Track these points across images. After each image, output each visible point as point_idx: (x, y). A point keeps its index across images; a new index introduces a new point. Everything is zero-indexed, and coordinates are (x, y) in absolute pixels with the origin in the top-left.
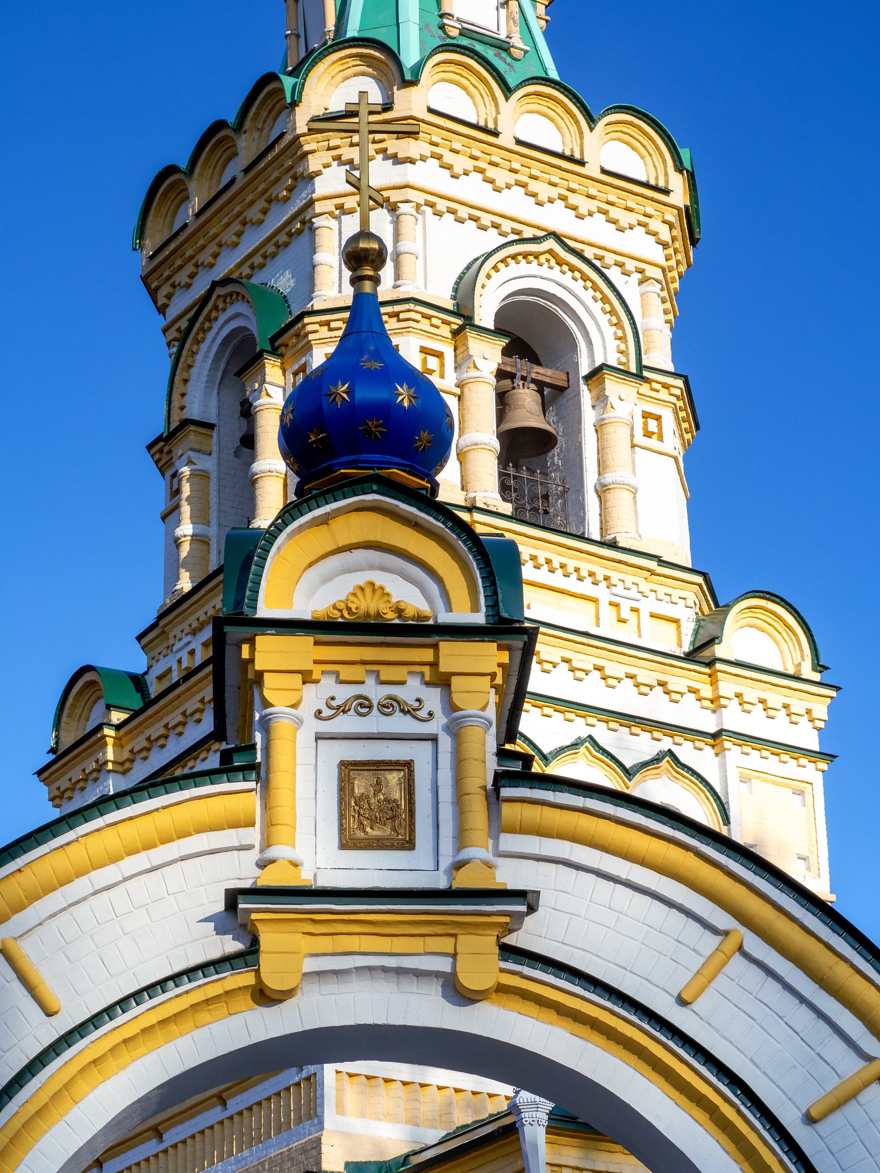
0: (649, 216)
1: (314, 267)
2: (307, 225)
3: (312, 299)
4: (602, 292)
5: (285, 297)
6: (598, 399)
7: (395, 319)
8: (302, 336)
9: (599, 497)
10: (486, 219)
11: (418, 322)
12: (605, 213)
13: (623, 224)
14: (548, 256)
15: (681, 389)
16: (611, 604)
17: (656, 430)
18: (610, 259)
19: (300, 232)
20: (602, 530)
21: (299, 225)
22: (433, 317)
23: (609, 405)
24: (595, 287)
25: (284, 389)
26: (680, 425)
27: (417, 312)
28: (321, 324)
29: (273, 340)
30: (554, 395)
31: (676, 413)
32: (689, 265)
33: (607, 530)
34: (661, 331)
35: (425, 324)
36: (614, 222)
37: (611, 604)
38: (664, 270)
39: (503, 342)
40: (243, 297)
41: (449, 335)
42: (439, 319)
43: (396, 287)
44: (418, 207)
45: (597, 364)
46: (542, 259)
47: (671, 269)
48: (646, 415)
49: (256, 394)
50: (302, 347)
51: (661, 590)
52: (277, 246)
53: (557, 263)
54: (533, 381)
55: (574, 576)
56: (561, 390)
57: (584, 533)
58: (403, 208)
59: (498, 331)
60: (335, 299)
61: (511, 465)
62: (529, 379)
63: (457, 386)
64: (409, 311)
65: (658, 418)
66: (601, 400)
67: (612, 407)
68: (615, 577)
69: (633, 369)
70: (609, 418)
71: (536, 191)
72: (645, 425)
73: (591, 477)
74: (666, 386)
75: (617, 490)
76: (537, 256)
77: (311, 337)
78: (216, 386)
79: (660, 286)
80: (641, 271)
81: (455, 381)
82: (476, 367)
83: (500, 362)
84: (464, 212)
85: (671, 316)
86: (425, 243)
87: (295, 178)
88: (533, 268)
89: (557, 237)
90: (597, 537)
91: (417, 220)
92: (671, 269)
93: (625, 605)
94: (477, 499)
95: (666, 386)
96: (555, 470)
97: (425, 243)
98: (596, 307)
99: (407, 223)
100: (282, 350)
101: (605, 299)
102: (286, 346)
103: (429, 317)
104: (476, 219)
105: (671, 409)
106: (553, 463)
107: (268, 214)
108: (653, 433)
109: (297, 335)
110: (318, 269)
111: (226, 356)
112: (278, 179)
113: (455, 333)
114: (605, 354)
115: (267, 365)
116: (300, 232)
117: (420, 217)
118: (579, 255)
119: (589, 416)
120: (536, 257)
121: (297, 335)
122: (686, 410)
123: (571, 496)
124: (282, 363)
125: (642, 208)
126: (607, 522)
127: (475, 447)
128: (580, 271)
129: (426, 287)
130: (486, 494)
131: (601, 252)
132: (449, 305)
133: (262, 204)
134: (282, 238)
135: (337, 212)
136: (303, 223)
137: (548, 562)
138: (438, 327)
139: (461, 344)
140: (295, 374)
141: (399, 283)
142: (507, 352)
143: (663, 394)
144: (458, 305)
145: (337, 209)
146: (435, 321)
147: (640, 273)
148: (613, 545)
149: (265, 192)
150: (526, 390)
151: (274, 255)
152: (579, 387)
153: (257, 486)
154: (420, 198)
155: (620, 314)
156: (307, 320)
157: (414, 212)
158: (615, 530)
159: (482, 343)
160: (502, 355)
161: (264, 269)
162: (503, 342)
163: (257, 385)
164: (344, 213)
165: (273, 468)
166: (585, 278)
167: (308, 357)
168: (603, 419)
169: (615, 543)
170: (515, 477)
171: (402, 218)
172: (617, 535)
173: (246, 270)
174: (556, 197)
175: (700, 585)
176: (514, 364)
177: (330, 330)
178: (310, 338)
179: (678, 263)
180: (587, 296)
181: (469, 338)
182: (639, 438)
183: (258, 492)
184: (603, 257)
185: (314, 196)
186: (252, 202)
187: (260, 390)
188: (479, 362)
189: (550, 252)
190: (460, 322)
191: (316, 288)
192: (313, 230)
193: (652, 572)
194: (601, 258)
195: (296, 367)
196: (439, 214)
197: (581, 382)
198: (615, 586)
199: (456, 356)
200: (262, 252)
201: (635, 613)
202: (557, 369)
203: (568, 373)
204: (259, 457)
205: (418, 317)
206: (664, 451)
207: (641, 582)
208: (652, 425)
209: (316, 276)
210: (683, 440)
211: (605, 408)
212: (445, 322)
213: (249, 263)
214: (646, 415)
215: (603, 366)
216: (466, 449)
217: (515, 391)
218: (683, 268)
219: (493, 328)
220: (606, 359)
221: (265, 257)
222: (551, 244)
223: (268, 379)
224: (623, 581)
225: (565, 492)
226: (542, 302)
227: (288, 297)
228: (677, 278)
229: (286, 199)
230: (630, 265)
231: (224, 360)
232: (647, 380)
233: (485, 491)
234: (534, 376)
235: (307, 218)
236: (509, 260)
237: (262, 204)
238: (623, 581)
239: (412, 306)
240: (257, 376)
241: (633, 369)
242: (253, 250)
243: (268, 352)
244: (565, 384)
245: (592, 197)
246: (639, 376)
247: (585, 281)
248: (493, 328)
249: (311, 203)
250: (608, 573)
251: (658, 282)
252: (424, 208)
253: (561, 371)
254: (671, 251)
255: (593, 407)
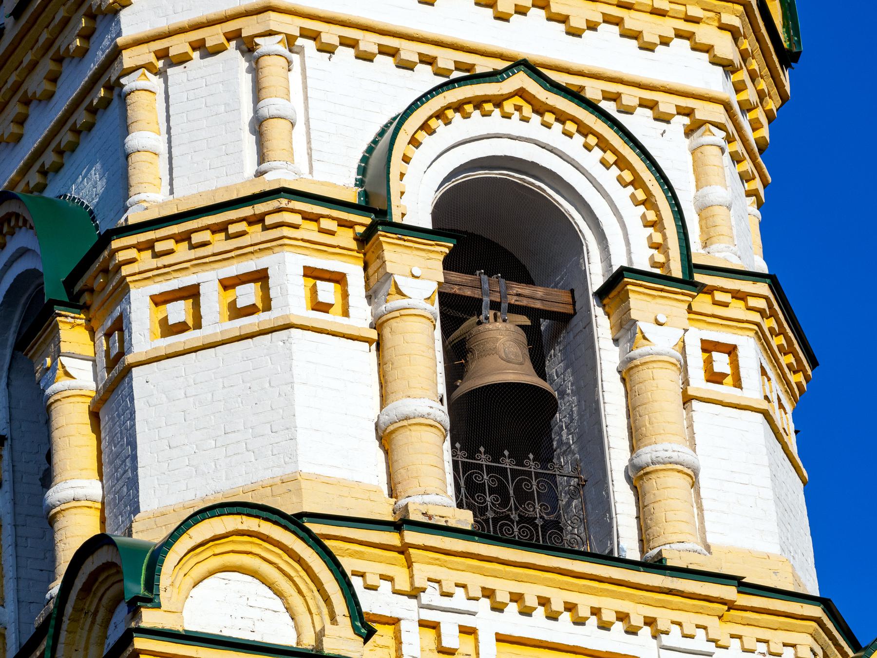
0: (696, 21)
1: (127, 156)
2: (116, 91)
3: (126, 209)
4: (615, 152)
5: (91, 212)
6: (621, 326)
7: (259, 227)
8: (111, 271)
9: (634, 488)
10: (410, 51)
11: (296, 227)
12: (618, 22)
13: (650, 37)
14: (518, 101)
15: (767, 298)
16: (423, 624)
17: (727, 370)
18: (631, 97)
19: (106, 103)
20: (643, 542)
21: (102, 93)
22: (323, 216)
23: (639, 335)
24: (604, 144)
25: (94, 361)
26: (777, 360)
27: (293, 211)
28: (140, 247)
29: (70, 282)
30: (553, 332)
31: (762, 337)
32: (784, 98)
33: (649, 541)
34: (729, 208)
35: (309, 231)
36: (635, 36)
37: (423, 624)
38: (728, 107)
39: (444, 248)
40: (25, 221)
41: (354, 245)
42: (333, 219)
43: (259, 174)
44: (290, 41)
45: (615, 269)
46: (508, 106)
47: (746, 108)
48: (708, 347)
49: (49, 374)
50: (115, 289)
51: (750, 634)
52: (77, 132)
53: (535, 111)
54: (514, 309)
55: (593, 621)
56: (562, 320)
57: (612, 551)
58: (265, 45)
59: (436, 233)
60: (161, 206)
61: (482, 449)
62: (504, 306)
63: (373, 326)
64: (279, 210)
65: (731, 350)
66: (626, 329)
67: (645, 338)
68: (664, 618)
69: (677, 271)
70: (641, 356)
71: (712, 43)
72: (709, 362)
73: (618, 457)
74: (738, 295)
75: (661, 474)
76: (498, 102)
77: (125, 270)
78: (5, 374)
79: (724, 134)
80: (688, 113)
81: (370, 320)
82: (400, 293)
83: (442, 280)
84: (369, 42)
85: (757, 184)
86: (306, 98)
87: (92, 16)
88: (495, 122)
89: (531, 68)
90: (633, 553)
91: (289, 63)
92: (746, 108)
93: (450, 626)
94: (411, 509)
95: (738, 295)
96: (564, 453)
97: (306, 98)
98: (609, 178)
99: (272, 68)
100: (86, 298)
101: (622, 163)
102: (91, 291)
103: (316, 218)
104: (393, 53)
105: (752, 334)
106: (560, 442)
107: (59, 82)
108: (725, 375)
109: (105, 271)
110: (133, 158)
111: (14, 324)
112: (66, 22)
113: (363, 240)
114: (629, 252)
115: (61, 325)
116: (106, 103)
117: (295, 58)
118: (576, 96)
119: (609, 357)
120: (498, 105)
121: (105, 271)
122: (782, 332)
123: (590, 491)
124: (88, 320)
125: (682, 8)
126: (648, 528)
127: (405, 423)
128: (574, 120)
129: (311, 172)
130: (426, 498)
131: (613, 88)
132: (352, 195)
133: (47, 65)
134: (81, 117)
135: (160, 64)
136: (109, 88)
137: (544, 602)
138: (332, 233)
139: (374, 256)
140: (108, 335)
141: (265, 166)
142: (449, 264)
143: (737, 310)
144: (366, 195)
145: (158, 59)
146: (325, 224)
147: (687, 115)
148: (657, 565)
149: (50, 44)
150: (499, 325)
151: (73, 147)
152: (589, 310)
153: (57, 526)
154: (291, 25)
155: (649, 184)
156: (115, 244)
157: (283, 49)
158: (662, 540)
159: (408, 251)
160: (444, 269)
161: (63, 171)
162: (444, 248)
163: (49, 361)
164: (172, 64)
165: (80, 493)
166: (584, 130)
167: (124, 304)
168: (632, 359)
169: (661, 560)
170: (490, 469)
171: (264, 61)
172: (663, 548)
173: (34, 178)
174: (672, 34)
175: (818, 621)
176: (477, 284)
177: (156, 255)
178: (124, 273)
179: (761, 95)
180: (592, 160)
181: (385, 246)
182: (698, 383)
183: (58, 537)
184: (398, 50)
185: (120, 41)
186: (34, 65)
187: (53, 368)
188: (404, 283)
189: (521, 93)
190: (367, 221)
191: (133, 191)
192: (123, 97)
193: (731, 606)
194: (615, 98)
195: (109, 323)
196: (327, 50)
197: (593, 301)
198: (667, 633)
199: (367, 279)
200: (53, 145)
201: (431, 633)
202: (556, 286)
203: (572, 291)
204: (57, 479)
205: (296, 219)
206: (743, 403)
207: (712, 622)
208: (721, 362)
209: (131, 171)
210: (788, 383)
211: (632, 340)
212: (342, 224)
213: (37, 166)
214: (708, 347)
215: (623, 272)
216: (392, 428)
217: (481, 328)
218: (772, 104)
219: (429, 225)
220: (630, 260)
221: (60, 152)
222: (521, 80)
223: (64, 348)
224: (680, 624)
225: (581, 486)
226: (516, 177)
227: (96, 212)
228: (764, 120)
229: (83, 53)
230: (668, 104)
231: (13, 329)
232: (701, 288)
233: (425, 493)
234: (513, 300)
235: (113, 78)
236: (450, 113)
237: (47, 65)
238: (680, 624)
239: (283, 202)
240: (49, 346)
241: (677, 271)
242: (41, 143)
243: (61, 304)
244: (568, 309)
245: (662, 13)
246: (688, 283)
247: (586, 136)
248: (429, 225)
249: (116, 53)
250: (651, 612)
251: (720, 127)
252: (300, 42)
253: (563, 288)
254: (743, 75)
255: (616, 341)
